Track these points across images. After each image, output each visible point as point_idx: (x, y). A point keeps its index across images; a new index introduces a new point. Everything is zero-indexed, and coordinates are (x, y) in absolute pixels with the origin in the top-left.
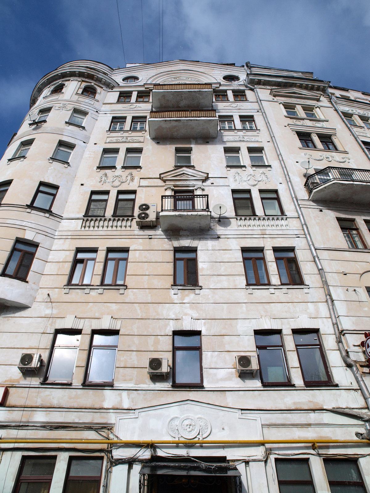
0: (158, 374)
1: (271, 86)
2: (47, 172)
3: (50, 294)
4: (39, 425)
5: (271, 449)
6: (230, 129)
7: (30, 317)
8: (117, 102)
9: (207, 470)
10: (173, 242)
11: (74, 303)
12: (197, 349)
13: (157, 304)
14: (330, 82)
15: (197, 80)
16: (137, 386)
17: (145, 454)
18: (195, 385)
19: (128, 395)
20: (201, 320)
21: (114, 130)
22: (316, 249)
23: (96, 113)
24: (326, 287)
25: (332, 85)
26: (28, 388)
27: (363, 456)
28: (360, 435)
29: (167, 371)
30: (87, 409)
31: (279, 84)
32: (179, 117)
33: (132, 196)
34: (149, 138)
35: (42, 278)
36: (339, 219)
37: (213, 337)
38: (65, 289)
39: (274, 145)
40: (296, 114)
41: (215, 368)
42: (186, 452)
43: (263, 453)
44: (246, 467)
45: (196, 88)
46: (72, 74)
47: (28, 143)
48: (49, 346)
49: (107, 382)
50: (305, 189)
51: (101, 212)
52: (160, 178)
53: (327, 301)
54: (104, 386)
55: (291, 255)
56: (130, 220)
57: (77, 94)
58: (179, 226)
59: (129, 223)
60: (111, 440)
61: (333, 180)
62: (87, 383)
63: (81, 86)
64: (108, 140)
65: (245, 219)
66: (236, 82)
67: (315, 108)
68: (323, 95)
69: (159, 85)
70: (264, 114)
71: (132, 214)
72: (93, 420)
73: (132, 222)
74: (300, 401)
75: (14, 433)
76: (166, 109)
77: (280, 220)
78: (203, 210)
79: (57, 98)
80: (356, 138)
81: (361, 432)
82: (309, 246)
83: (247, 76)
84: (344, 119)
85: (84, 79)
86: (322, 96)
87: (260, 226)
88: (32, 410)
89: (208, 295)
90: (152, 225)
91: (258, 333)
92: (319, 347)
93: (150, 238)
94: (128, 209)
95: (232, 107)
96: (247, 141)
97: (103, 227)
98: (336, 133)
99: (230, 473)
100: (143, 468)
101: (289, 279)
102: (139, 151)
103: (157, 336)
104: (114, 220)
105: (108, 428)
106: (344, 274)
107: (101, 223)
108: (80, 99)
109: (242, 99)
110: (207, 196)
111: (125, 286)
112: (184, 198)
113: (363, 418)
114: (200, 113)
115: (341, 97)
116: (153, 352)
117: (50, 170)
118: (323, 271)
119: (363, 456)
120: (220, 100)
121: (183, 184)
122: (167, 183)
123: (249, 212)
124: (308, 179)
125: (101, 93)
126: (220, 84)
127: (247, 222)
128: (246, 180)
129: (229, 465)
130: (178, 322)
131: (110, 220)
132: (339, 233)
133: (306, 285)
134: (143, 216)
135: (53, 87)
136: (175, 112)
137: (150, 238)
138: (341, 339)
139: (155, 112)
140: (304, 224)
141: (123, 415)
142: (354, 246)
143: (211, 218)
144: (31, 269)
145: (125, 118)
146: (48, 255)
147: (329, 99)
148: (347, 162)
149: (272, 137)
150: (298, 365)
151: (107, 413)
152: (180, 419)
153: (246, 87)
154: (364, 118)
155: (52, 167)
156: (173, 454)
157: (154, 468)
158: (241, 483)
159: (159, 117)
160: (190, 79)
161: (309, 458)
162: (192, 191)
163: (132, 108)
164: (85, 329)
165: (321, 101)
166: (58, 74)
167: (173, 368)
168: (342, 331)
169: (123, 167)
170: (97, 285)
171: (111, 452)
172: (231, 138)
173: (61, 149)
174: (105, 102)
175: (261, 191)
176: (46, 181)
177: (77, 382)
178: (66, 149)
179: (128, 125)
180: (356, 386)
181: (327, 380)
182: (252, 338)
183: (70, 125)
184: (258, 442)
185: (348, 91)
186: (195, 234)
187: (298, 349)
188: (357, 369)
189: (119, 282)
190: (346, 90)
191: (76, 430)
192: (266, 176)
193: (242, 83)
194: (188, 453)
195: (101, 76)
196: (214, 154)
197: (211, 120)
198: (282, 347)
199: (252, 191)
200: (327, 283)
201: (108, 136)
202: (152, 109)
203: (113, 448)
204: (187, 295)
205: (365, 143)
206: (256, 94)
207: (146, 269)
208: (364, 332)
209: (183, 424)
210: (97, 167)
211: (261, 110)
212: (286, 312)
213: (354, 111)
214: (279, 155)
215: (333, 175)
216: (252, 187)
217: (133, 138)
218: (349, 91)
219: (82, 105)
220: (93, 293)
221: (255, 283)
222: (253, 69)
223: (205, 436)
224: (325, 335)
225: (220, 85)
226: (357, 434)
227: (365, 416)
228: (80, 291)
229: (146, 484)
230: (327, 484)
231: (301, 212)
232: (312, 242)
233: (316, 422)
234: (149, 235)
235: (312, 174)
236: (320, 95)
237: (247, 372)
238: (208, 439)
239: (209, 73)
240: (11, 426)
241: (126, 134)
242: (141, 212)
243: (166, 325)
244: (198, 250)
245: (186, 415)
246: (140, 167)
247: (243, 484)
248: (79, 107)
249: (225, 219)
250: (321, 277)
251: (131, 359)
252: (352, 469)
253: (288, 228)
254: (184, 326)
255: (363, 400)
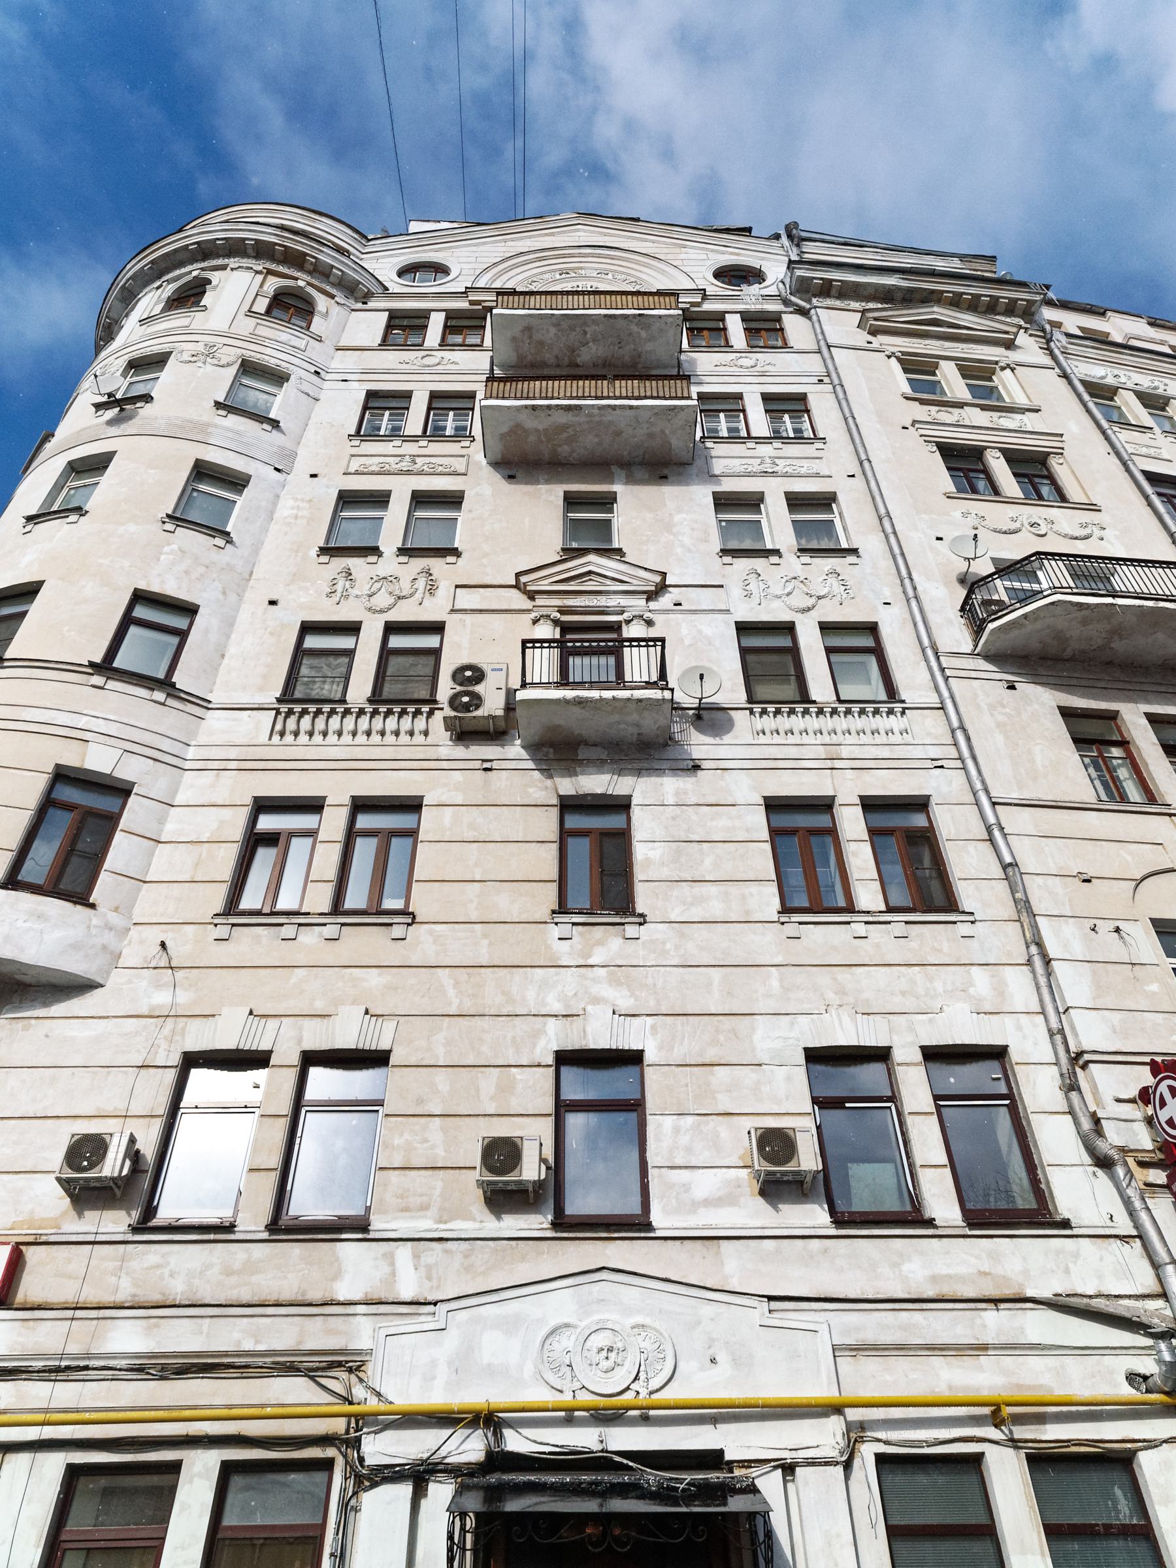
0: (509, 1188)
1: (862, 301)
2: (159, 560)
3: (167, 943)
4: (123, 1363)
5: (862, 1426)
6: (734, 437)
7: (100, 1018)
8: (380, 345)
9: (665, 1494)
10: (558, 780)
11: (245, 970)
12: (629, 1108)
13: (509, 969)
14: (1048, 287)
15: (633, 280)
16: (443, 1226)
17: (467, 1446)
18: (624, 1221)
19: (416, 1256)
20: (644, 1017)
21: (373, 433)
22: (994, 804)
23: (314, 378)
24: (1027, 920)
25: (1054, 298)
26: (90, 1247)
27: (1151, 1444)
28: (1141, 1380)
29: (537, 1178)
30: (281, 1305)
31: (887, 296)
32: (578, 398)
33: (431, 641)
34: (484, 461)
35: (143, 892)
36: (1067, 713)
37: (681, 1068)
38: (216, 925)
39: (869, 487)
40: (938, 390)
41: (686, 1167)
42: (596, 1438)
43: (839, 1438)
44: (785, 1482)
45: (630, 306)
46: (235, 249)
47: (96, 465)
48: (162, 1108)
49: (347, 1218)
50: (963, 621)
51: (335, 687)
52: (516, 586)
53: (1029, 963)
54: (340, 1230)
55: (919, 820)
56: (425, 715)
57: (251, 312)
58: (577, 732)
59: (420, 723)
60: (359, 1404)
61: (1049, 592)
62: (284, 1221)
63: (265, 288)
64: (355, 465)
65: (778, 712)
66: (755, 289)
67: (998, 369)
68: (1026, 329)
69: (514, 292)
70: (838, 388)
71: (431, 695)
72: (300, 1343)
73: (430, 720)
74: (951, 1271)
75: (37, 1393)
76: (539, 372)
77: (884, 715)
78: (649, 685)
79: (186, 324)
80: (1125, 464)
81: (1142, 1371)
82: (975, 795)
83: (788, 268)
84: (1091, 405)
85: (273, 267)
86: (1022, 331)
87: (821, 734)
88: (100, 1316)
89: (664, 943)
90: (492, 730)
91: (814, 1056)
92: (1007, 1102)
93: (486, 769)
94: (417, 681)
95: (741, 367)
96: (786, 475)
97: (340, 734)
98: (1063, 449)
99: (736, 1504)
100: (460, 1492)
101: (911, 895)
102: (454, 500)
103: (508, 1069)
104: (375, 713)
105: (350, 1364)
106: (1085, 881)
107: (335, 722)
108: (262, 331)
109: (770, 343)
110: (660, 643)
111: (408, 915)
112: (590, 646)
113: (1150, 1327)
114: (642, 385)
115: (1081, 334)
116: (495, 1119)
117: (168, 554)
118: (1016, 869)
119: (1151, 1444)
120: (704, 344)
121: (587, 603)
122: (540, 601)
123: (789, 690)
124: (971, 591)
125: (330, 312)
126: (705, 295)
127: (784, 722)
128: (779, 593)
129: (732, 1478)
130: (572, 1021)
131: (362, 712)
132: (1068, 754)
133: (964, 912)
134: (471, 701)
135: (170, 286)
136: (563, 382)
137: (486, 769)
138: (1077, 1080)
139: (500, 380)
140: (959, 728)
141: (398, 1321)
142: (1115, 794)
143: (673, 709)
144: (106, 866)
145: (407, 395)
146: (162, 821)
147: (1044, 341)
148: (1094, 536)
149: (864, 462)
150: (943, 1159)
151: (346, 1318)
152: (578, 1330)
153: (786, 302)
154: (1154, 402)
155: (175, 547)
156: (557, 1446)
157: (495, 1493)
158: (769, 1534)
159: (513, 395)
160: (610, 276)
161: (983, 1454)
162: (616, 627)
163: (429, 366)
164: (282, 1050)
165: (1019, 347)
166: (187, 245)
167: (557, 1168)
168: (1080, 1054)
169: (402, 551)
170: (320, 912)
171: (356, 1443)
172: (736, 465)
173: (203, 487)
174: (343, 343)
175: (826, 628)
176: (155, 587)
177: (253, 1221)
178: (221, 488)
179: (414, 421)
180: (1124, 1226)
181: (1034, 1206)
182: (800, 1074)
183: (229, 412)
184: (821, 1401)
185: (1103, 314)
186: (626, 755)
187: (943, 1110)
188: (1129, 1171)
189: (389, 904)
190: (1101, 313)
191: (244, 1375)
192: (842, 583)
193: (772, 291)
194: (602, 1442)
195: (327, 257)
196: (684, 515)
197: (675, 407)
198: (893, 1102)
199: (799, 629)
200: (1030, 907)
201: (355, 451)
202: (492, 370)
203: (365, 1430)
204: (600, 943)
205: (1152, 478)
206: (817, 325)
207: (474, 862)
208: (1147, 1059)
209: (586, 1347)
210: (321, 549)
211: (830, 377)
212: (903, 994)
213: (1123, 380)
214: (883, 518)
215: (1052, 576)
216: (799, 615)
217: (433, 460)
218: (1109, 314)
219: (268, 351)
220: (309, 937)
221: (806, 904)
222: (808, 247)
223: (655, 1384)
224: (1027, 1066)
225: (705, 297)
226: (1133, 1378)
227: (1156, 1321)
228: (266, 932)
229: (469, 1545)
230: (1039, 1532)
231: (949, 689)
232: (983, 782)
233: (1003, 1340)
234: (484, 761)
235: (985, 574)
236: (1014, 330)
237: (785, 1178)
238: (666, 1395)
239: (669, 257)
240: (30, 1369)
241: (410, 448)
242: (459, 688)
243: (536, 1034)
244: (632, 806)
245: (596, 1317)
246: (455, 552)
247: (777, 1539)
248: (259, 356)
249: (714, 712)
250: (1011, 888)
251: (426, 1141)
252: (1116, 1488)
253: (908, 738)
254: (590, 1037)
255: (1150, 1271)
